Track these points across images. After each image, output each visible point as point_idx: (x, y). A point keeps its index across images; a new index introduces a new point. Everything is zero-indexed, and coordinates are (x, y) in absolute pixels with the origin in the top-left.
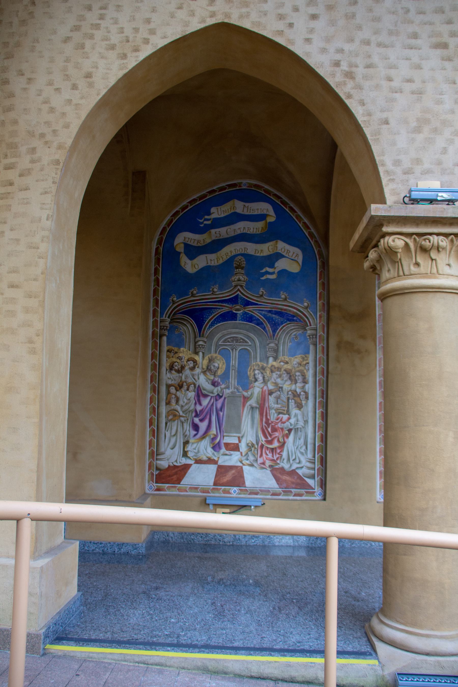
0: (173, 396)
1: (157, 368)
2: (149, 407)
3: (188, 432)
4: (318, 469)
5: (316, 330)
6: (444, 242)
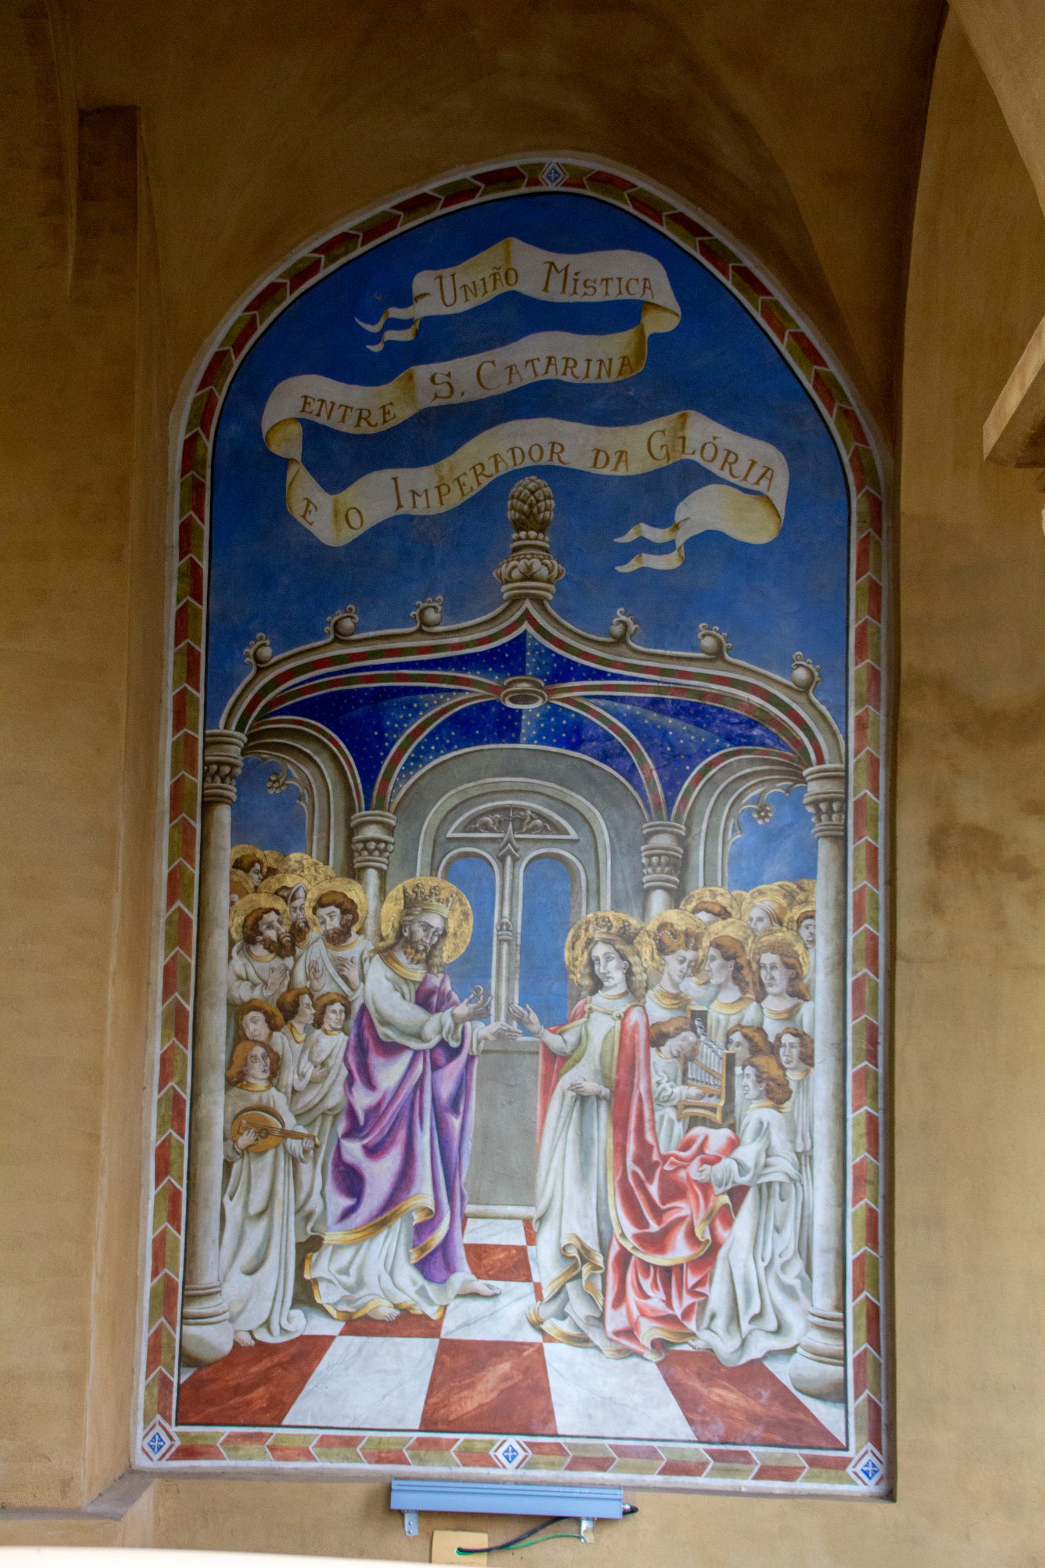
0: (259, 1051)
1: (189, 934)
2: (156, 1097)
3: (316, 1197)
4: (859, 1362)
5: (843, 779)
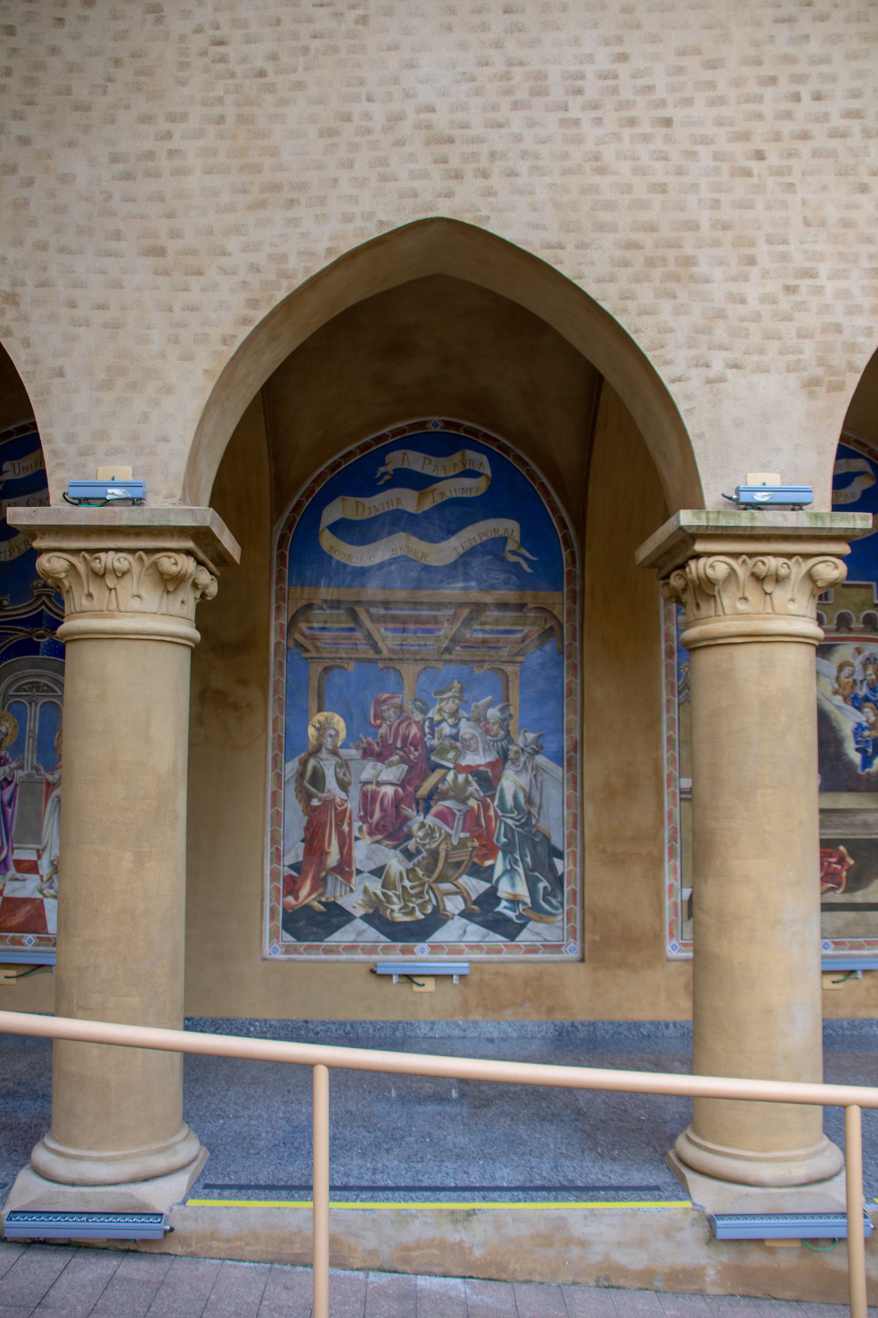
6: (122, 562)
